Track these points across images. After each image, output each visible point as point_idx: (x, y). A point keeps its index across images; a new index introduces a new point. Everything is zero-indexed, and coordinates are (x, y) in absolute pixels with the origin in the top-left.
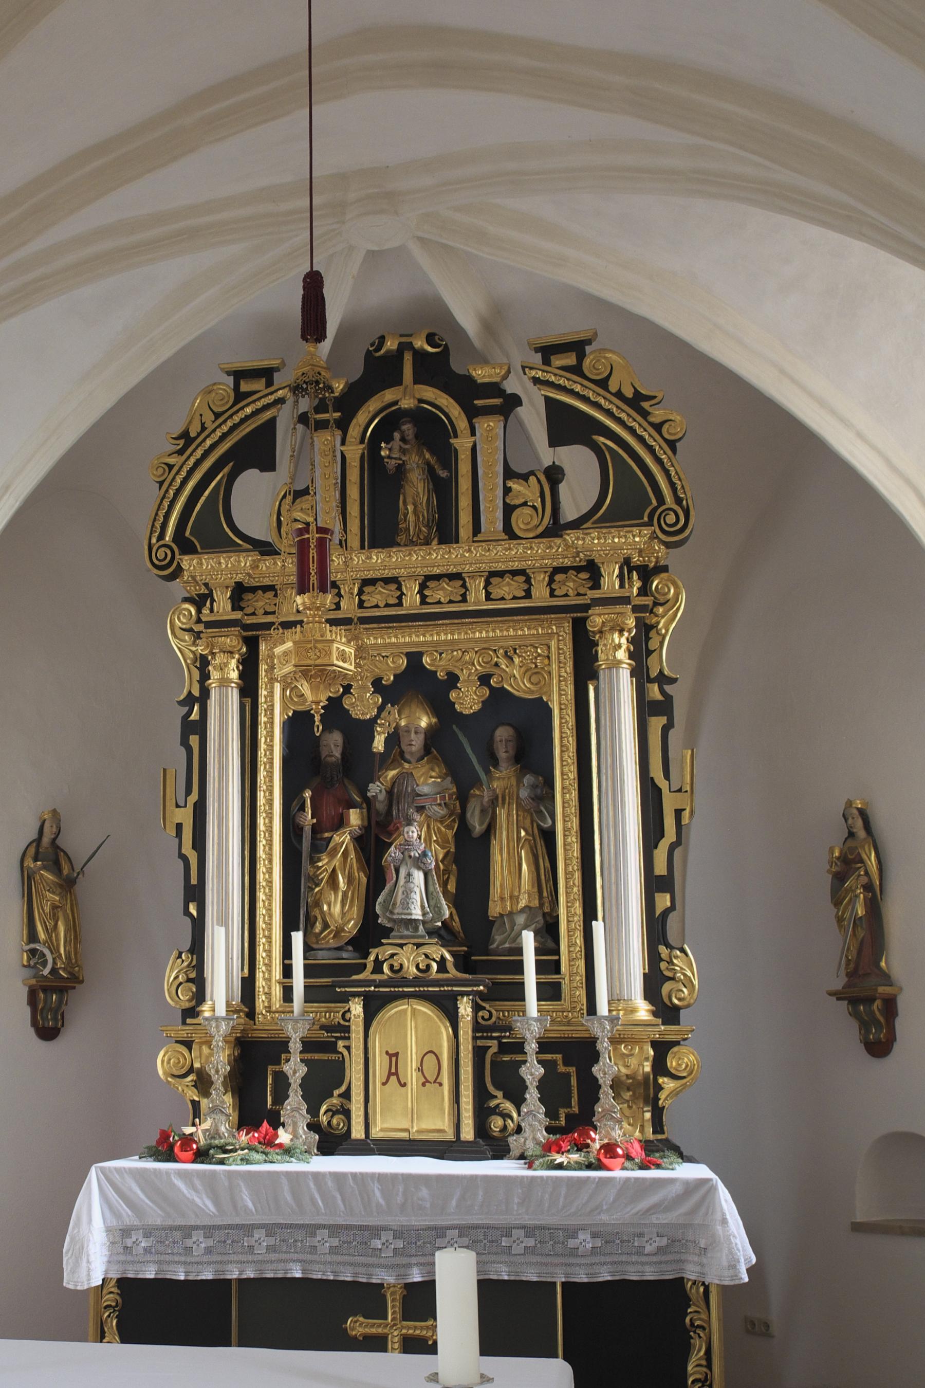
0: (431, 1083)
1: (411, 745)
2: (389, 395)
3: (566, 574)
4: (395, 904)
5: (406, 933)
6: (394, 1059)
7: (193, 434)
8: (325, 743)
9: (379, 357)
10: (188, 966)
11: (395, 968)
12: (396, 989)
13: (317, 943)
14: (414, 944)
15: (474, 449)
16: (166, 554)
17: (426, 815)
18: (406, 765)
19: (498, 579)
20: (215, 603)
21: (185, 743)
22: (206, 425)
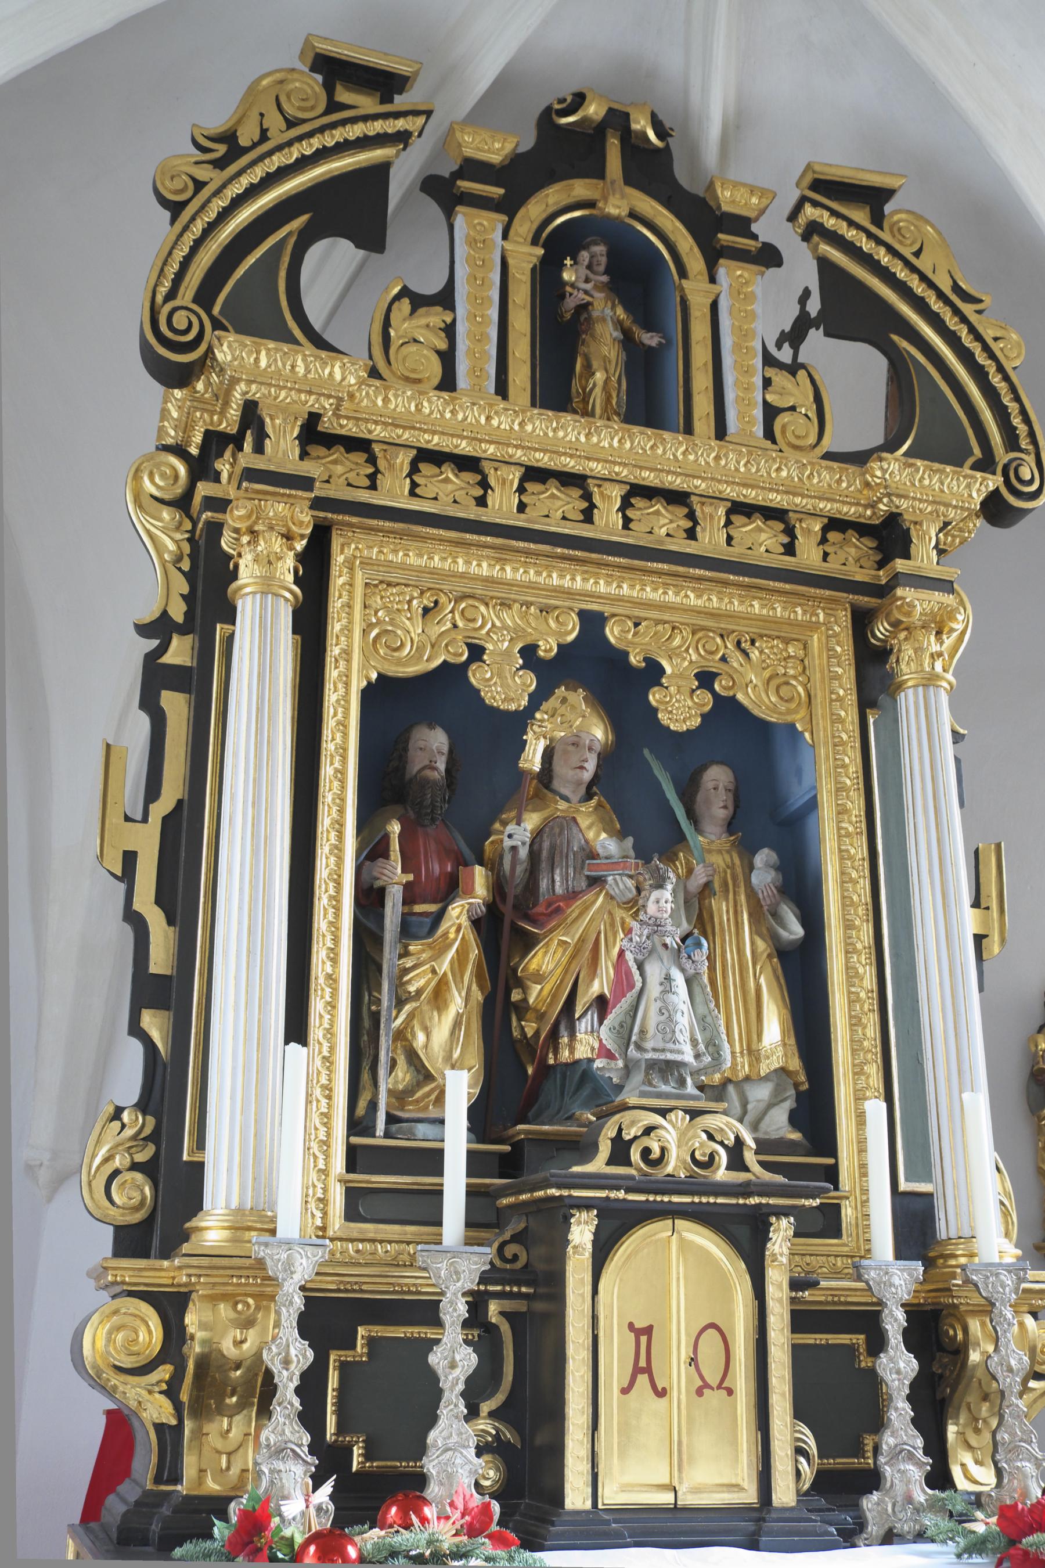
0: (712, 1389)
1: (582, 768)
2: (581, 189)
3: (844, 533)
4: (643, 1032)
5: (664, 1088)
6: (644, 1339)
7: (244, 141)
8: (421, 744)
9: (559, 127)
10: (134, 1137)
12: (659, 1198)
13: (402, 1110)
14: (686, 1111)
15: (714, 306)
16: (190, 324)
17: (607, 894)
18: (562, 805)
19: (742, 519)
20: (267, 441)
21: (150, 703)
22: (269, 134)
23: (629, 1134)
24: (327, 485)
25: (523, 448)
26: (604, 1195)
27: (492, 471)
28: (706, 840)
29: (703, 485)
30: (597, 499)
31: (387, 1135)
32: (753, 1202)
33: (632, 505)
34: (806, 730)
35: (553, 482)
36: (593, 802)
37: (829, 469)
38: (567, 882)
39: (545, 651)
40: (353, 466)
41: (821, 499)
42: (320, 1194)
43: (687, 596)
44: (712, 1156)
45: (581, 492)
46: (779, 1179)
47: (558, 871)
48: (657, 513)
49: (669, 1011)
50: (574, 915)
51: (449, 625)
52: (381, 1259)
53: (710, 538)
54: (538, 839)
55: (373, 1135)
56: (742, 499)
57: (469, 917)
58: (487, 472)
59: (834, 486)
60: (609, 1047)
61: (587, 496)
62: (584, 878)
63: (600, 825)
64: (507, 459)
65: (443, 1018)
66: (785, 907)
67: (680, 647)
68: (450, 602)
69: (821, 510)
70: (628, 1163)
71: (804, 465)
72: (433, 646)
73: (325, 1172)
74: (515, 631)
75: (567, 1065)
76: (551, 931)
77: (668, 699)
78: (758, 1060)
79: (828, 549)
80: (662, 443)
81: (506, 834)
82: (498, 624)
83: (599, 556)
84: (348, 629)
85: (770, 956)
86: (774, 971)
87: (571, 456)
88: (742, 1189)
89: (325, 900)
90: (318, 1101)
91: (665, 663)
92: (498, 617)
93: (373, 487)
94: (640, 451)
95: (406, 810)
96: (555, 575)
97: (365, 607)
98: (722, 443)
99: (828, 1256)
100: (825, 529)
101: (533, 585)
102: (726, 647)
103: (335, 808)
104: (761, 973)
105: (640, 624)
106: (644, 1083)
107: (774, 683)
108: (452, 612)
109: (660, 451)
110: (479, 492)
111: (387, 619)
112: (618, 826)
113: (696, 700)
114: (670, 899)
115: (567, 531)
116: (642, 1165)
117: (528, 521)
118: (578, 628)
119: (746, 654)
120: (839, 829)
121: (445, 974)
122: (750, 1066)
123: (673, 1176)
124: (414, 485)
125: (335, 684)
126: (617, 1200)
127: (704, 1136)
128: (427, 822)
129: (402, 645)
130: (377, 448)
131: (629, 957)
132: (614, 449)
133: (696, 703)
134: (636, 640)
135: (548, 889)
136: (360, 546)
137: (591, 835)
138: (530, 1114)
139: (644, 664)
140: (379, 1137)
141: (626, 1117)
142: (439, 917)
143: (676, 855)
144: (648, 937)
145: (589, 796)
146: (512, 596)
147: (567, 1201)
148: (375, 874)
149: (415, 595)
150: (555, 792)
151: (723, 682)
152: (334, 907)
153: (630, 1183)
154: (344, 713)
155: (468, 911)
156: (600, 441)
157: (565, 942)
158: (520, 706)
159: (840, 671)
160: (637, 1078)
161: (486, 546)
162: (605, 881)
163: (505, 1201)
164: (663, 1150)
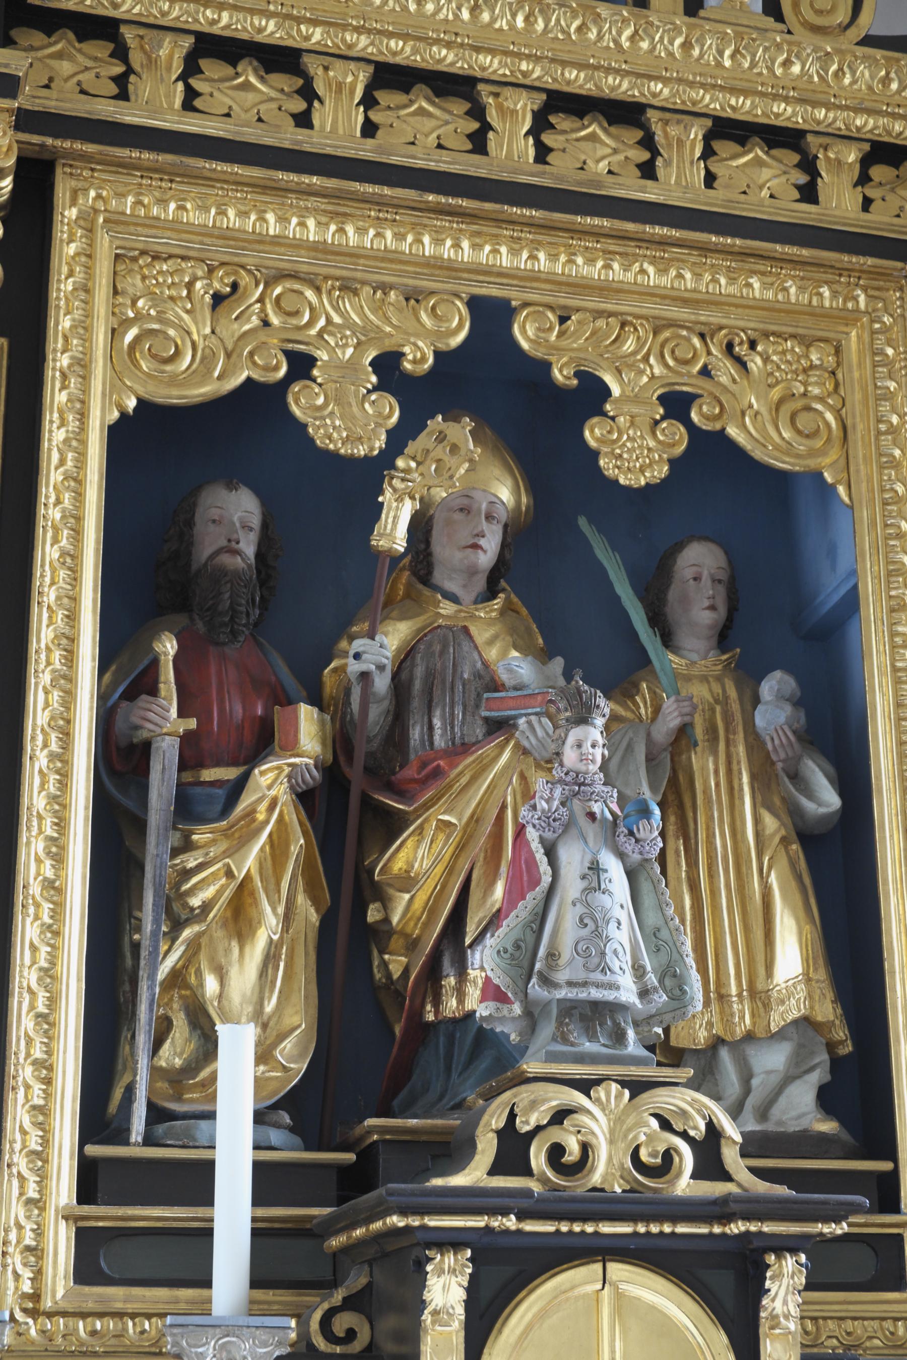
1: (476, 546)
3: (897, 168)
4: (552, 955)
5: (589, 1046)
8: (214, 513)
11: (568, 1159)
13: (179, 1098)
14: (623, 1084)
17: (518, 745)
18: (447, 608)
23: (527, 1123)
24: (45, 93)
25: (369, 32)
26: (482, 1224)
27: (320, 71)
28: (683, 662)
29: (666, 91)
30: (492, 117)
31: (149, 1140)
32: (736, 1231)
33: (552, 126)
34: (839, 482)
35: (420, 89)
36: (498, 603)
37: (873, 63)
38: (452, 728)
39: (414, 362)
40: (90, 64)
41: (857, 110)
42: (29, 1239)
43: (643, 271)
44: (668, 1156)
45: (467, 106)
46: (782, 1190)
47: (437, 713)
48: (592, 137)
49: (595, 921)
50: (464, 780)
51: (255, 321)
52: (132, 1345)
53: (678, 177)
54: (408, 663)
55: (126, 1142)
56: (729, 113)
57: (292, 787)
58: (312, 71)
59: (878, 87)
60: (496, 981)
61: (477, 112)
62: (480, 722)
63: (509, 638)
64: (344, 51)
65: (247, 949)
66: (810, 764)
67: (634, 353)
68: (257, 285)
69: (858, 129)
70: (528, 1172)
71: (828, 54)
72: (228, 355)
73: (37, 1204)
74: (364, 330)
75: (454, 1021)
76: (426, 806)
77: (615, 436)
78: (767, 1006)
79: (871, 193)
80: (595, 22)
81: (352, 653)
82: (337, 319)
83: (497, 207)
84: (84, 327)
85: (784, 841)
86: (793, 864)
87: (449, 45)
88: (717, 1210)
89: (42, 760)
90: (28, 1087)
91: (609, 379)
92: (337, 309)
93: (123, 95)
94: (560, 36)
95: (192, 620)
96: (426, 239)
97: (116, 292)
98: (692, 20)
99: (884, 1319)
100: (866, 162)
101: (390, 256)
102: (709, 353)
103: (60, 614)
104: (770, 868)
105: (569, 318)
106: (554, 1039)
107: (787, 410)
108: (261, 300)
109: (592, 35)
110: (300, 105)
111: (153, 312)
112: (540, 641)
113: (661, 438)
114: (601, 741)
115: (443, 167)
116: (550, 1174)
117: (379, 150)
118: (467, 325)
119: (741, 363)
120: (893, 634)
121: (248, 876)
122: (753, 1015)
123: (602, 1190)
124: (191, 95)
125: (61, 413)
126: (507, 1232)
127: (654, 1124)
128: (223, 638)
129: (178, 353)
130: (128, 34)
131: (532, 835)
132: (518, 32)
133: (659, 442)
134: (564, 343)
135: (422, 741)
136: (104, 193)
137: (492, 654)
138: (396, 1103)
139: (575, 382)
140: (136, 1144)
141: (523, 1095)
142: (238, 788)
143: (636, 686)
144: (563, 804)
145: (491, 592)
146: (359, 275)
147: (420, 1236)
148: (135, 720)
149: (200, 273)
150: (436, 588)
151: (705, 408)
152: (58, 772)
153: (524, 1203)
154: (76, 460)
155: (289, 777)
156: (493, 20)
157: (448, 824)
158: (372, 449)
159: (892, 385)
160: (547, 1030)
161: (310, 192)
162: (515, 727)
163: (336, 1242)
164: (585, 1147)
